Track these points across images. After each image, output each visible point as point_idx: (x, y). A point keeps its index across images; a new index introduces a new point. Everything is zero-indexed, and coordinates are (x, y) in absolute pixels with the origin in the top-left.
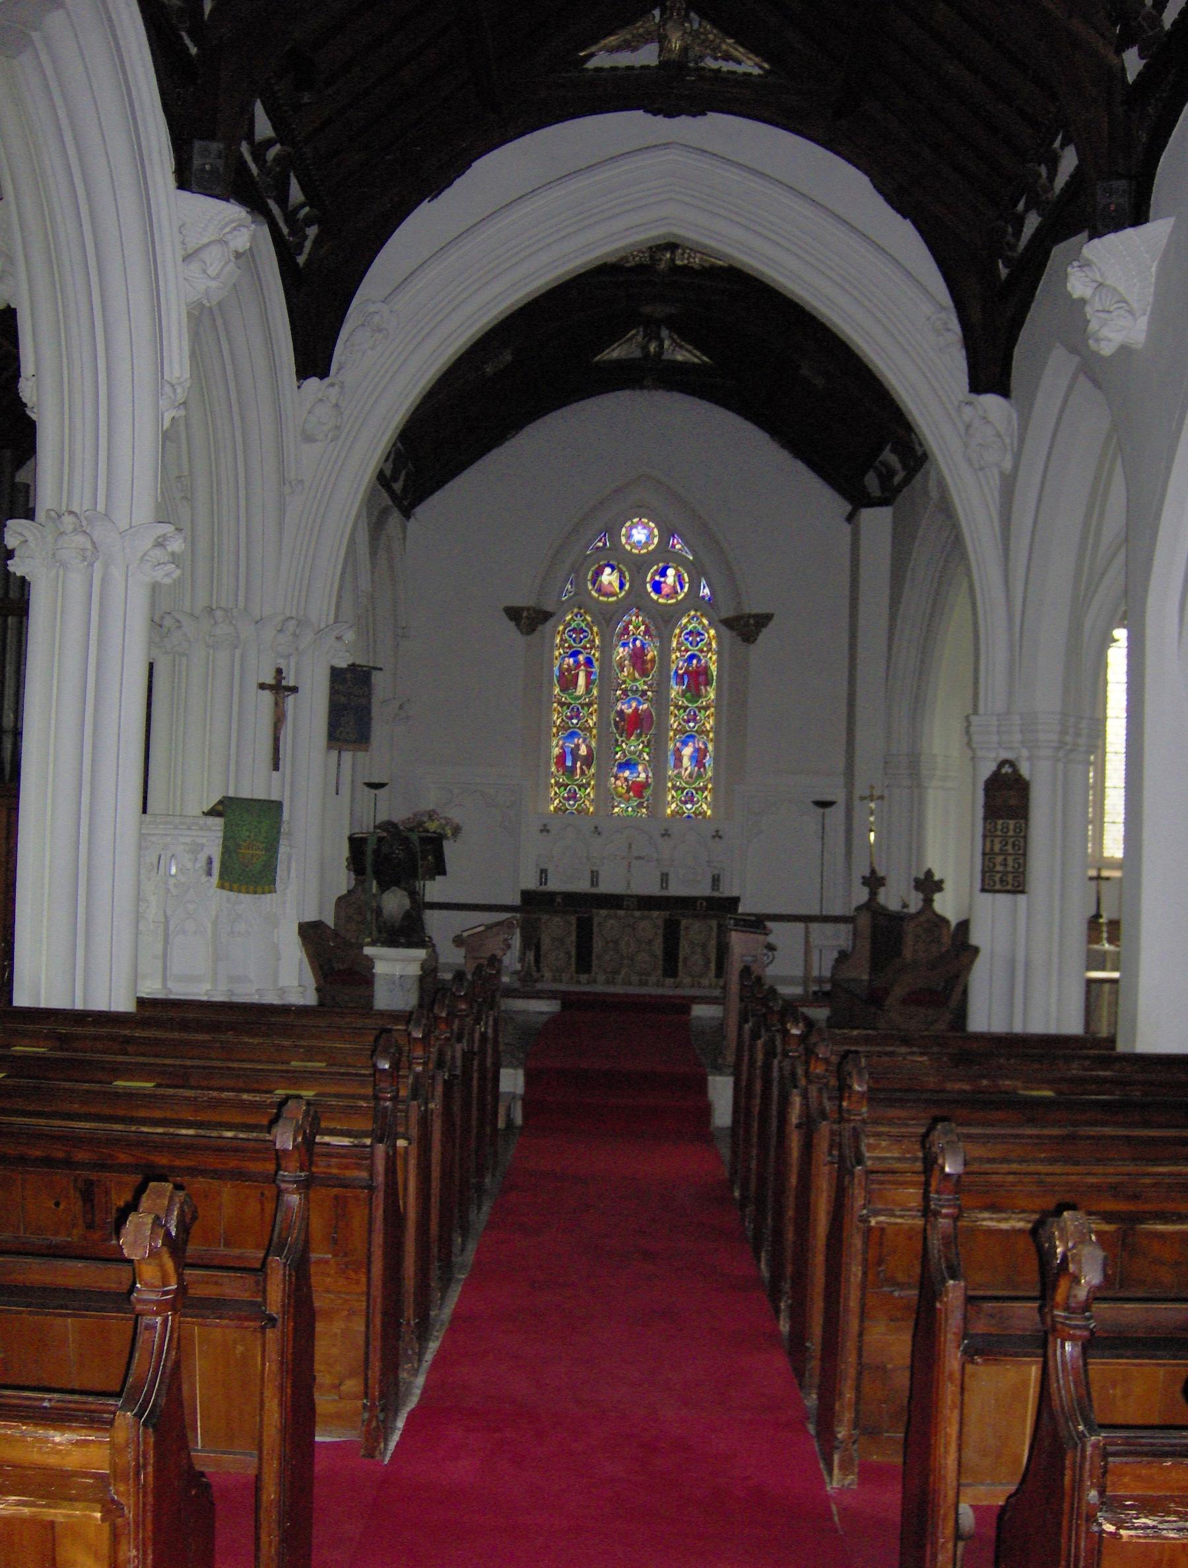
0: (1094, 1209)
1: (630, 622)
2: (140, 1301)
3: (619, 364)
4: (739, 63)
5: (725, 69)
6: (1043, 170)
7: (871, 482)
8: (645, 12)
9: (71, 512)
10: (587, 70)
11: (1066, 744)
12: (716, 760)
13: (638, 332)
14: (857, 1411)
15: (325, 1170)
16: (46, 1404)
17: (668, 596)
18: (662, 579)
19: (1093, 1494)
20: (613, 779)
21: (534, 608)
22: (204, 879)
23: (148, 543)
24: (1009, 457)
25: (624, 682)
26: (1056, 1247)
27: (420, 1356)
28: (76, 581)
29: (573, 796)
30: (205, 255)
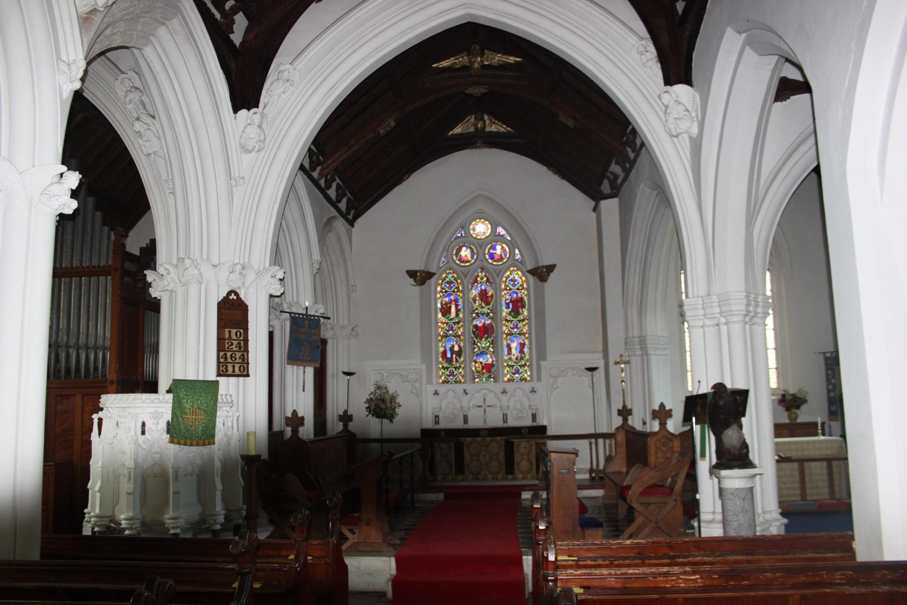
1: (478, 276)
3: (461, 136)
11: (750, 312)
12: (530, 348)
17: (498, 260)
18: (494, 252)
20: (473, 363)
21: (423, 271)
24: (696, 124)
25: (477, 309)
29: (452, 374)
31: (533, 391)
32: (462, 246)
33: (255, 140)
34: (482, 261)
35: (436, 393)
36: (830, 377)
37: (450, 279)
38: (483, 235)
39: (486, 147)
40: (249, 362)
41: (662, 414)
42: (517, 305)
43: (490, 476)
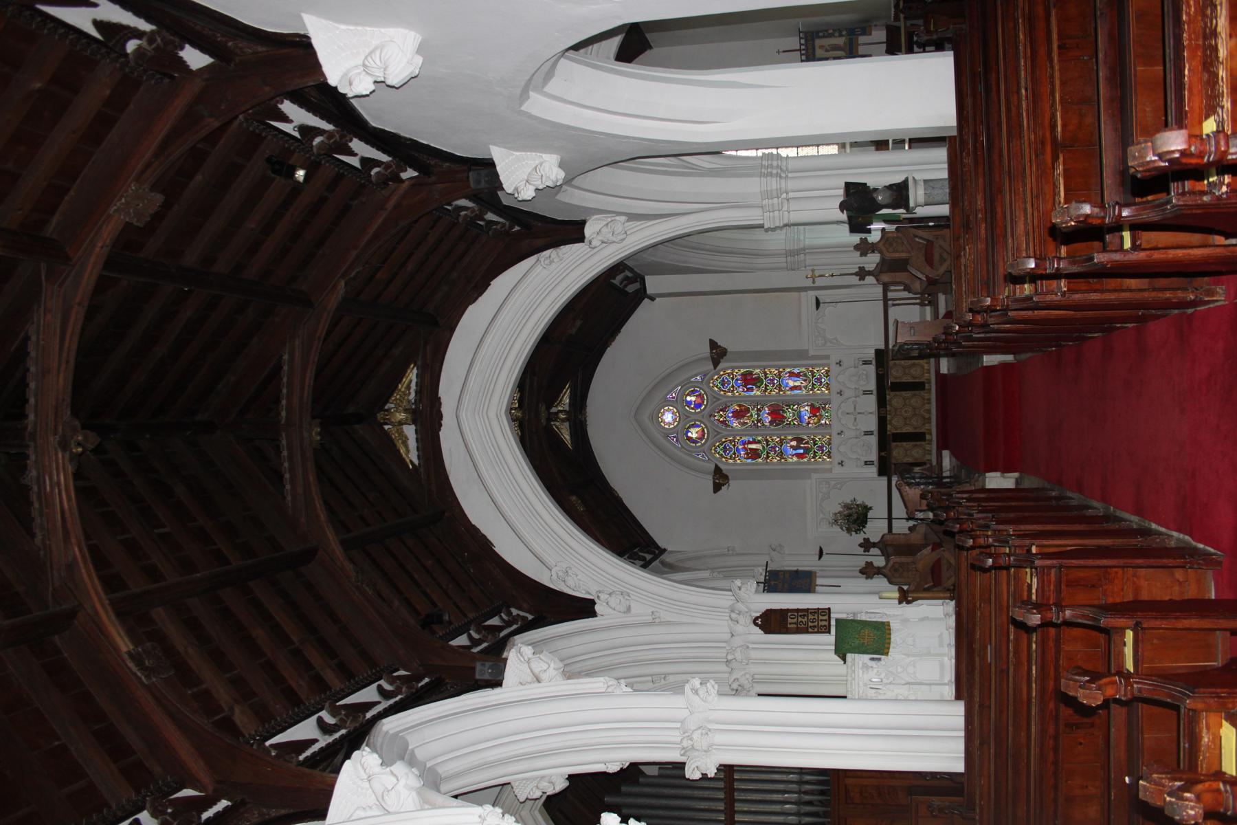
0: (1050, 165)
2: (1125, 695)
4: (411, 381)
5: (415, 388)
6: (463, 213)
7: (631, 288)
8: (387, 434)
9: (681, 741)
10: (419, 464)
12: (795, 366)
13: (555, 425)
14: (1178, 289)
15: (1052, 592)
16: (1187, 745)
19: (1205, 198)
20: (810, 425)
21: (714, 476)
22: (882, 662)
23: (696, 698)
24: (618, 218)
25: (753, 422)
26: (1071, 225)
27: (1160, 534)
28: (719, 738)
29: (821, 448)
30: (536, 671)
31: (839, 363)
32: (687, 436)
33: (622, 599)
34: (703, 416)
35: (841, 463)
36: (826, 34)
37: (721, 450)
38: (676, 415)
39: (585, 410)
40: (817, 607)
41: (864, 248)
42: (749, 380)
43: (927, 407)
